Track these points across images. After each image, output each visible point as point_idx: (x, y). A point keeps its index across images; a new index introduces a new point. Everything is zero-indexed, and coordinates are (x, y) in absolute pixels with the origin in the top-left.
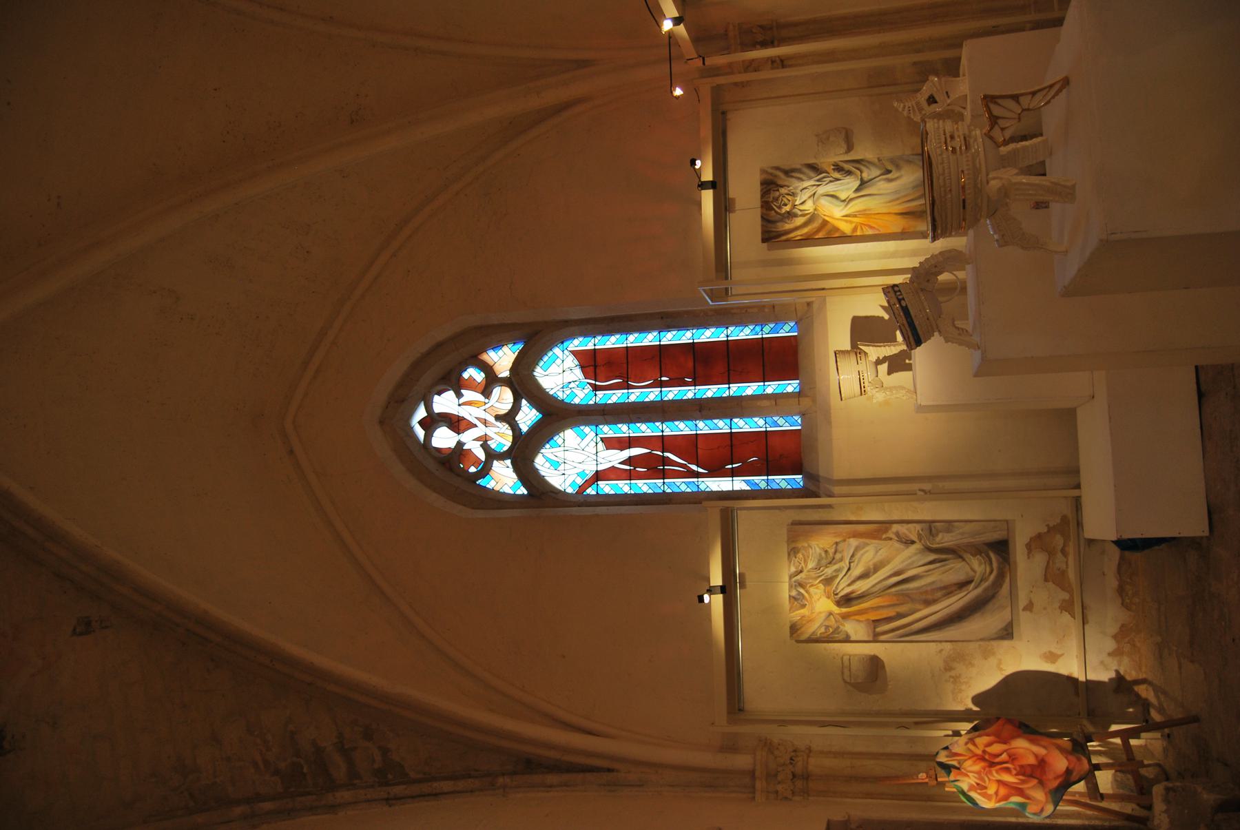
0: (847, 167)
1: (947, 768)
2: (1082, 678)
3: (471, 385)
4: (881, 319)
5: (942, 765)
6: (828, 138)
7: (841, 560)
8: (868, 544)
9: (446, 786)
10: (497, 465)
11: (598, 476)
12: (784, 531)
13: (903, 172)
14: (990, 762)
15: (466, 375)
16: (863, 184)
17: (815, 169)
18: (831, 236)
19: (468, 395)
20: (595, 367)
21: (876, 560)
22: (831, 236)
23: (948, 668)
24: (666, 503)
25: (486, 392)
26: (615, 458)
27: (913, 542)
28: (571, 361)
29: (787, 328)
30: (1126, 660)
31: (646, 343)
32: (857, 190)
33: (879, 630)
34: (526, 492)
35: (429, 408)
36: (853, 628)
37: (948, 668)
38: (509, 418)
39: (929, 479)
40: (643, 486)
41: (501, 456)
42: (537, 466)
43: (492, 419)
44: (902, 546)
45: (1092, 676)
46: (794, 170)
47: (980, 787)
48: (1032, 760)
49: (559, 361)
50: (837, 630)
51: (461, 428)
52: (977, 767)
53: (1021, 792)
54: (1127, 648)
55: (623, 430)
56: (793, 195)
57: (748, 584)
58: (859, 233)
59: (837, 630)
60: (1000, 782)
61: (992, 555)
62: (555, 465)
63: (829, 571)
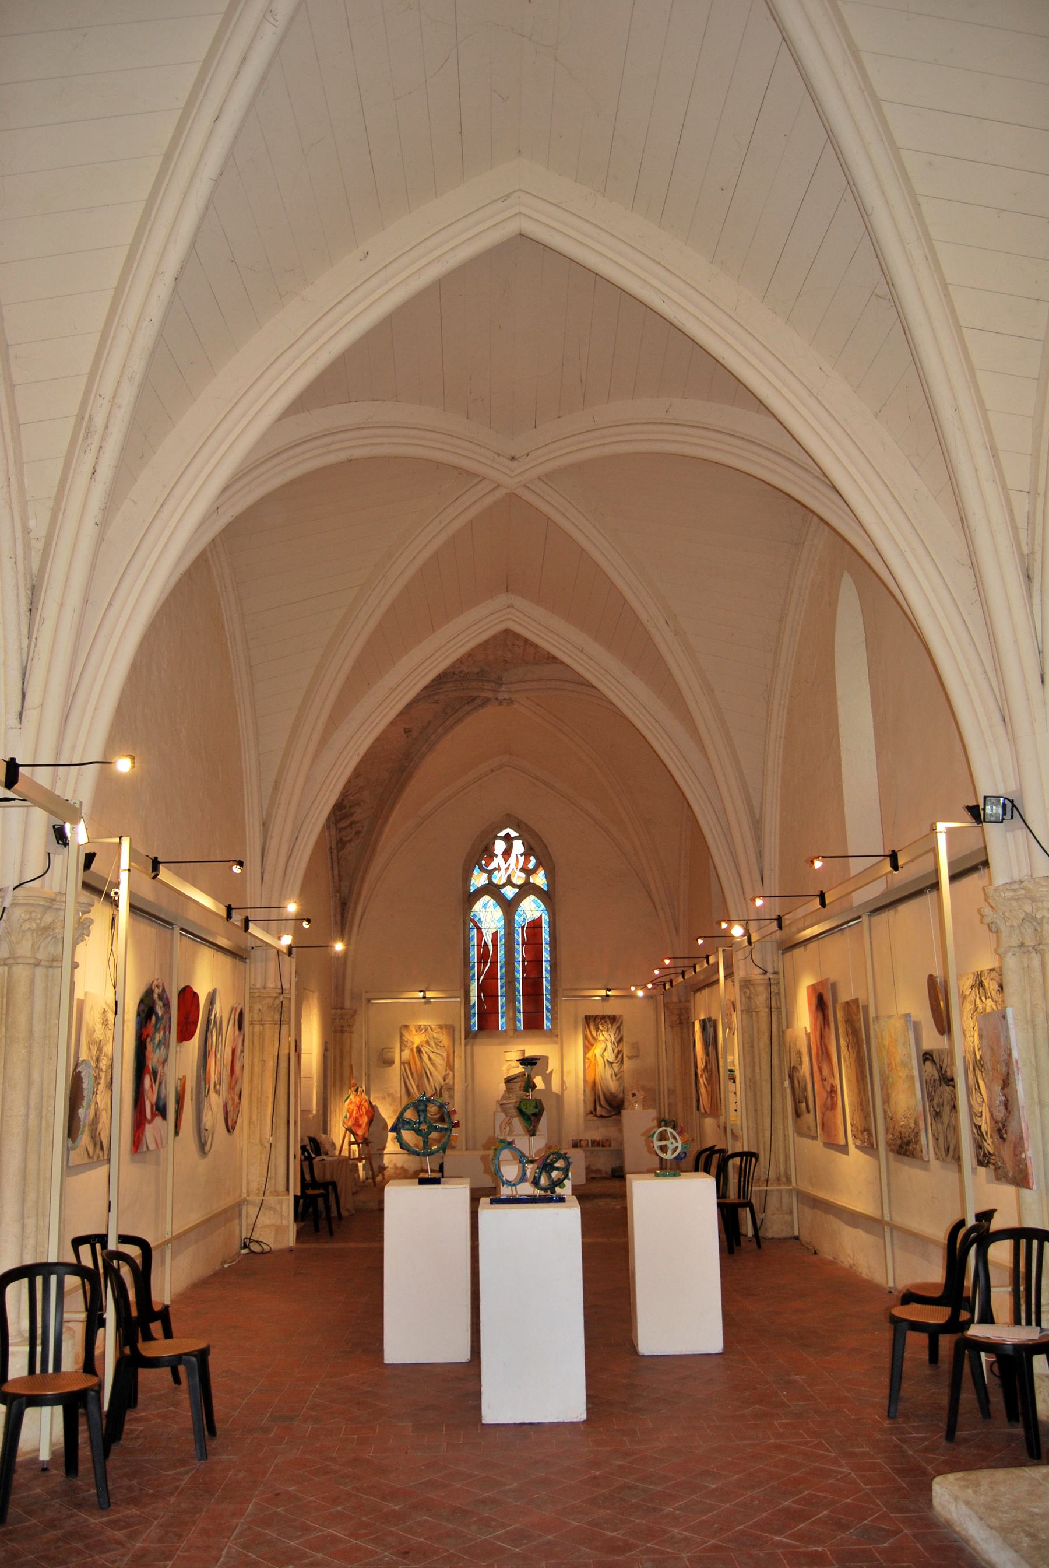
0: (620, 1056)
1: (357, 1091)
2: (385, 1152)
3: (527, 861)
4: (547, 1070)
5: (357, 1089)
6: (634, 1048)
7: (437, 1049)
8: (444, 1060)
9: (336, 872)
10: (485, 875)
11: (479, 929)
12: (451, 1023)
13: (615, 1082)
14: (359, 1107)
15: (532, 858)
16: (611, 1063)
17: (620, 1041)
18: (588, 1046)
19: (522, 859)
20: (534, 928)
21: (437, 1064)
22: (588, 1046)
23: (389, 1095)
24: (464, 964)
25: (523, 870)
26: (488, 938)
27: (445, 1081)
28: (537, 915)
29: (549, 1024)
30: (393, 1171)
31: (544, 954)
32: (608, 1061)
33: (406, 1065)
34: (471, 891)
35: (516, 838)
36: (406, 1054)
37: (389, 1095)
38: (509, 882)
39: (473, 1089)
40: (474, 953)
41: (489, 878)
42: (485, 897)
43: (508, 873)
44: (443, 1076)
45: (385, 1156)
46: (620, 1031)
47: (351, 1103)
48: (361, 1122)
49: (537, 909)
50: (406, 1046)
51: (505, 856)
52: (358, 1102)
53: (350, 1117)
54: (398, 1172)
55: (501, 942)
56: (607, 1031)
57: (427, 1006)
58: (586, 1061)
59: (406, 1046)
60: (353, 1110)
61: (438, 1116)
62: (485, 906)
63: (432, 1043)
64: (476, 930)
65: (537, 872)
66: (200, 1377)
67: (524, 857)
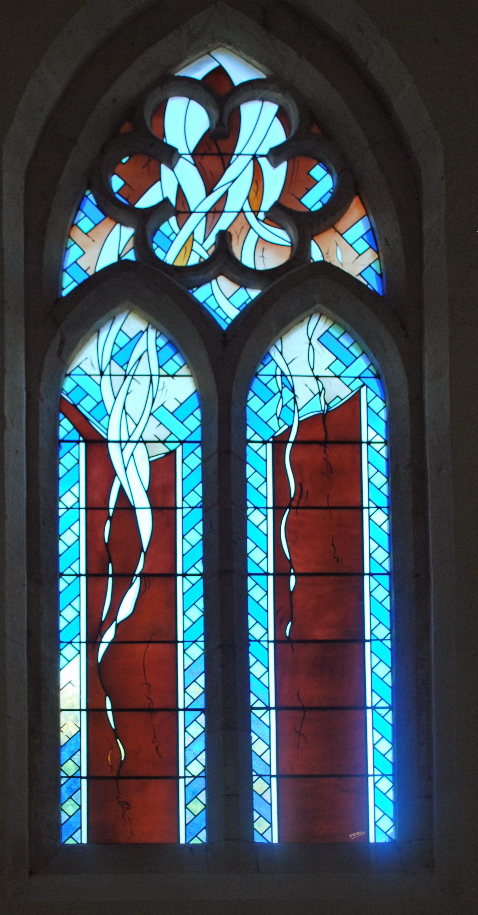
15: (318, 172)
20: (325, 443)
43: (224, 222)
49: (338, 368)
51: (207, 161)
64: (82, 445)
65: (341, 225)
66: (255, 59)
67: (283, 167)
